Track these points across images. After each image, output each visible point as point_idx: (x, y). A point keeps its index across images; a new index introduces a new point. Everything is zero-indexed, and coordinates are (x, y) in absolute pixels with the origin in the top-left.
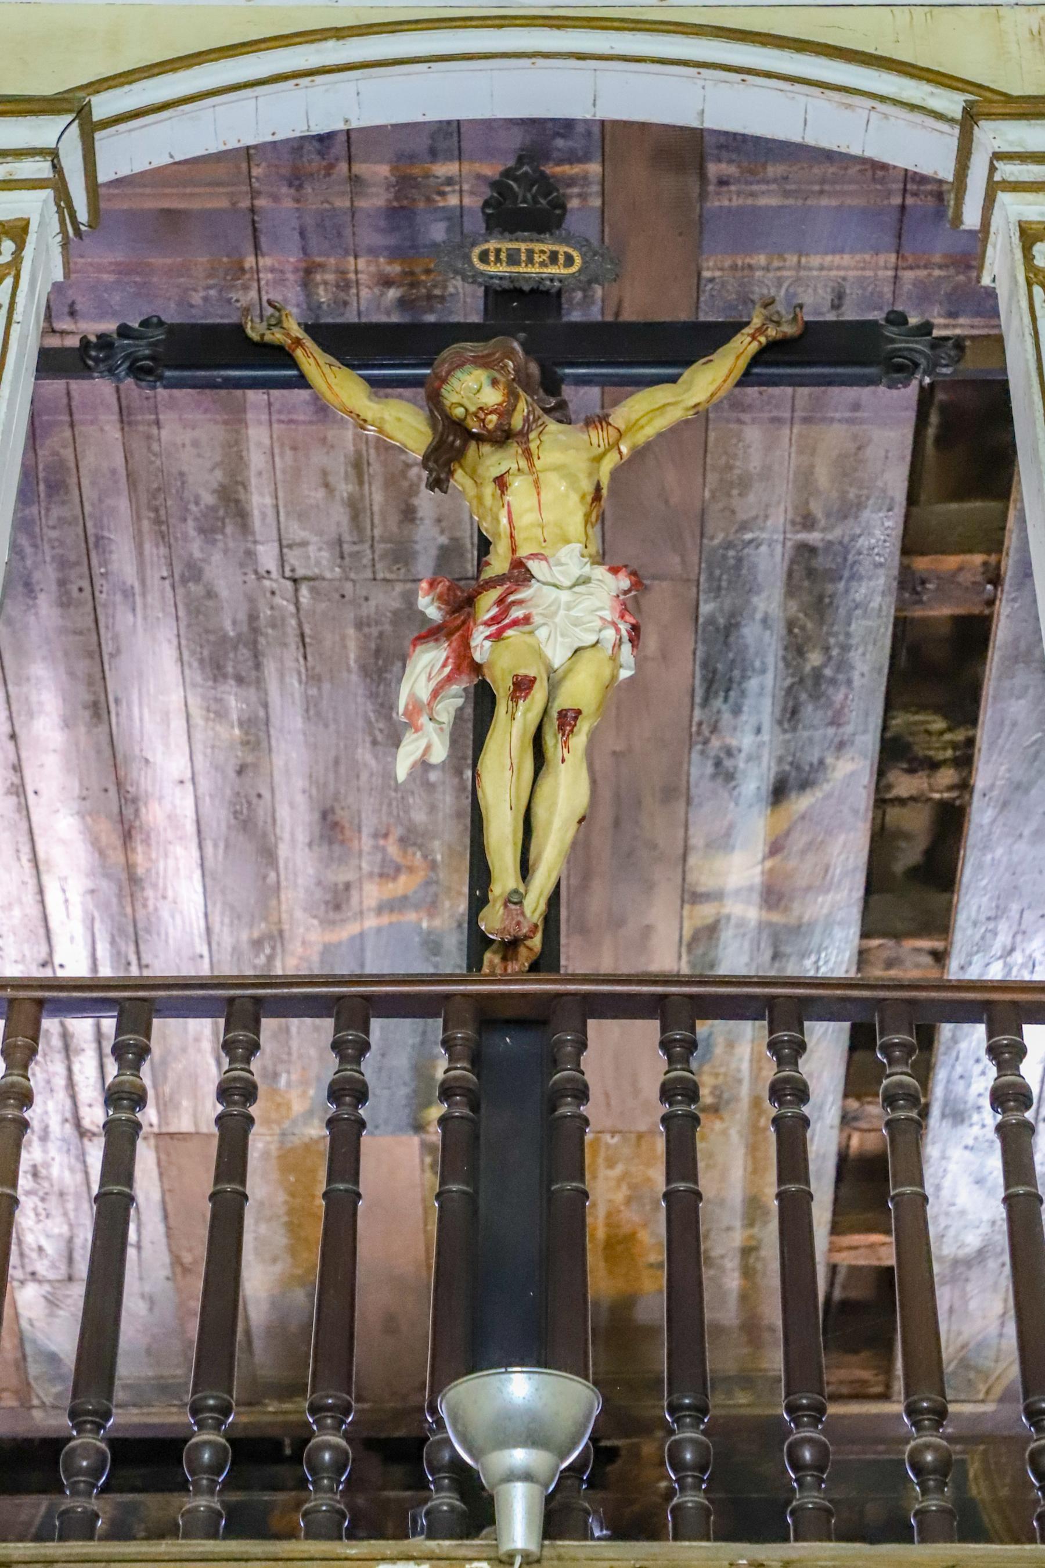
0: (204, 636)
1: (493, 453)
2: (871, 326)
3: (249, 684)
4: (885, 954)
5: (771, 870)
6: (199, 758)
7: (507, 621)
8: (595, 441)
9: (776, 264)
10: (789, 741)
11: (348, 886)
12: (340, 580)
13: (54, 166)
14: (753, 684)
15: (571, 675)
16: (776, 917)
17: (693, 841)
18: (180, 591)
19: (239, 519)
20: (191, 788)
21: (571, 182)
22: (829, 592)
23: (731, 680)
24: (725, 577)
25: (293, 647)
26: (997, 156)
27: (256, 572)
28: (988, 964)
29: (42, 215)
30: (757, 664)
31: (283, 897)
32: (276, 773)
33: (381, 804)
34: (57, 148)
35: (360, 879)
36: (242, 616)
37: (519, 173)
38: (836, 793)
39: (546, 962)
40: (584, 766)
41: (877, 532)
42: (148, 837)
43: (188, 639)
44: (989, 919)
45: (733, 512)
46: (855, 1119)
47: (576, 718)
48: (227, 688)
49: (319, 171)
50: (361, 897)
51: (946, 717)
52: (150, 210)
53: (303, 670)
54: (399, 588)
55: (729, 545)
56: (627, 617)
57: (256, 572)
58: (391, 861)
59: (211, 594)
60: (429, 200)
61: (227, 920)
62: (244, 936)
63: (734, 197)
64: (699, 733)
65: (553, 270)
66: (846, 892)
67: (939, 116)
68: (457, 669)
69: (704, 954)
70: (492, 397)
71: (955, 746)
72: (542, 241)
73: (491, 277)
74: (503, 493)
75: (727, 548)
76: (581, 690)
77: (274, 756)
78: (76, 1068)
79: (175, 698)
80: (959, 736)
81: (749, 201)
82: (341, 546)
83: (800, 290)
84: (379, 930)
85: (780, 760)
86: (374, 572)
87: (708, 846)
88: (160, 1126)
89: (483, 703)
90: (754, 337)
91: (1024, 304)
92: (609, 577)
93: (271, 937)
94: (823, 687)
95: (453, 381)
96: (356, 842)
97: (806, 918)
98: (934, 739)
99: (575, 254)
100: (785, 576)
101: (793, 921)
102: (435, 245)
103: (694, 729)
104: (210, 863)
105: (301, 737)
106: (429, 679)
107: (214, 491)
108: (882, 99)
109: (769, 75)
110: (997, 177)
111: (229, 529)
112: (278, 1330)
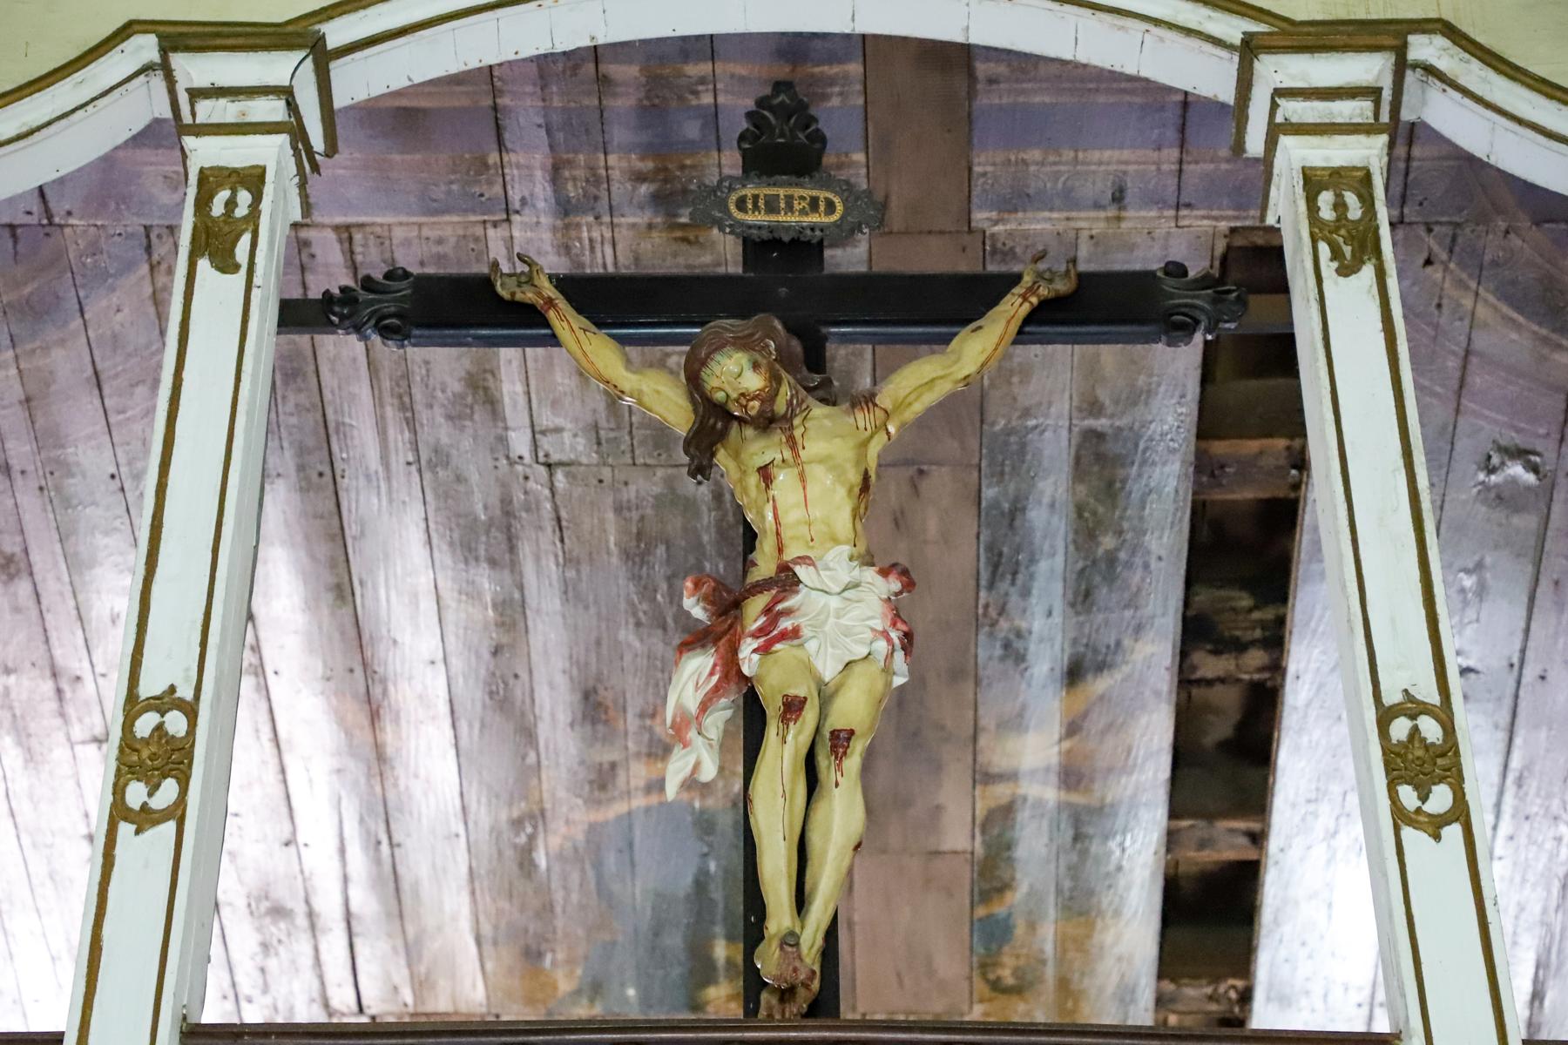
4: (1198, 833)
5: (1069, 752)
6: (451, 639)
8: (861, 424)
9: (1051, 158)
11: (613, 766)
13: (288, 104)
14: (1043, 566)
16: (1077, 798)
17: (983, 722)
18: (427, 476)
21: (832, 81)
25: (549, 530)
26: (1279, 93)
27: (508, 457)
28: (1309, 848)
29: (279, 163)
30: (1046, 547)
31: (544, 777)
32: (533, 655)
34: (291, 87)
35: (627, 759)
36: (494, 501)
37: (776, 101)
38: (1136, 675)
39: (824, 1005)
40: (859, 790)
41: (1170, 419)
44: (1309, 801)
45: (1015, 399)
46: (1173, 1000)
47: (849, 739)
48: (481, 570)
51: (1253, 594)
55: (1008, 432)
56: (900, 625)
57: (508, 457)
58: (660, 741)
59: (459, 479)
60: (681, 98)
61: (484, 800)
62: (504, 816)
64: (985, 614)
65: (814, 218)
67: (1217, 42)
68: (725, 677)
69: (1000, 835)
70: (754, 382)
71: (1263, 625)
72: (801, 186)
73: (750, 227)
74: (767, 487)
75: (1009, 435)
78: (323, 947)
79: (424, 580)
80: (1268, 614)
81: (1021, 99)
84: (648, 810)
85: (1075, 641)
86: (633, 458)
87: (998, 726)
88: (415, 1005)
89: (753, 721)
90: (1025, 299)
91: (1309, 264)
92: (879, 579)
93: (532, 817)
95: (712, 364)
97: (1109, 800)
98: (1241, 617)
99: (837, 200)
100: (1072, 462)
103: (981, 611)
104: (464, 742)
105: (559, 619)
106: (697, 688)
110: (1279, 119)
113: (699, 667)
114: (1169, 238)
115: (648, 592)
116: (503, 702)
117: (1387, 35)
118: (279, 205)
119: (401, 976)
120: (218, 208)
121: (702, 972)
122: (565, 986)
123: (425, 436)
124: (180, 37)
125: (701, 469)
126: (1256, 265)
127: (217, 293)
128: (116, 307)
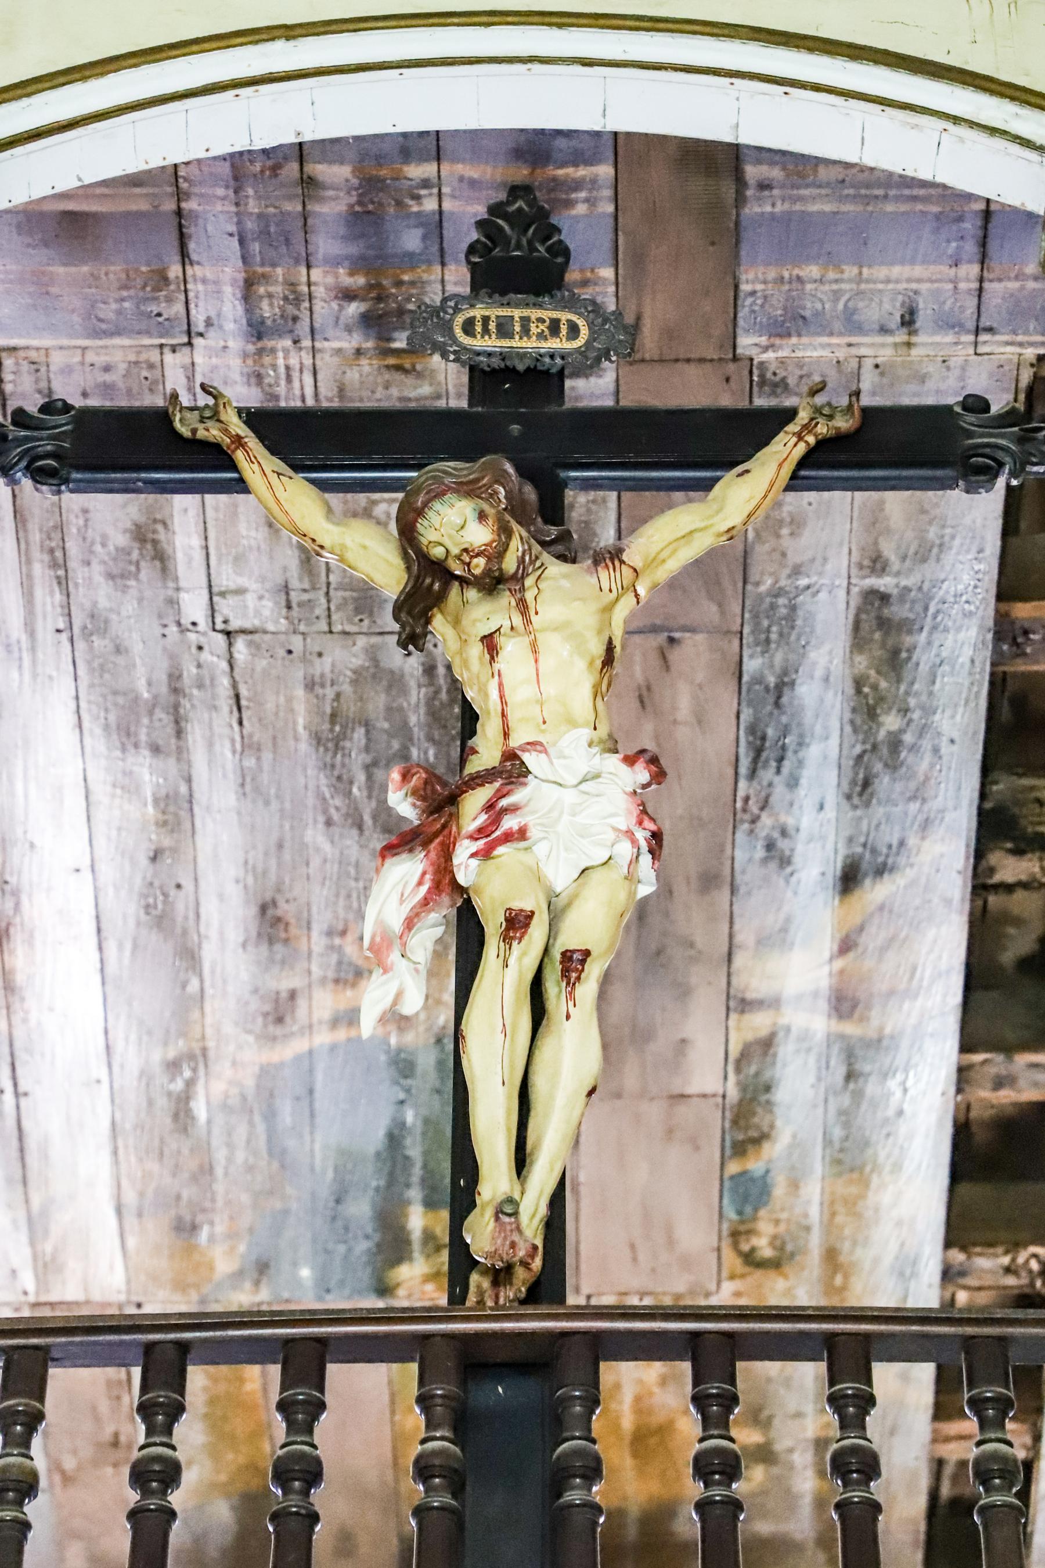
0: (110, 697)
1: (480, 600)
2: (942, 412)
3: (168, 755)
4: (993, 1070)
5: (842, 972)
6: (100, 842)
7: (498, 833)
8: (605, 586)
9: (831, 275)
10: (860, 818)
11: (293, 995)
12: (286, 633)
15: (576, 903)
16: (850, 1029)
17: (739, 938)
18: (80, 645)
19: (157, 563)
20: (90, 876)
21: (577, 185)
22: (907, 645)
23: (784, 748)
24: (774, 629)
25: (226, 709)
27: (179, 624)
31: (208, 1008)
33: (337, 895)
35: (310, 986)
39: (547, 1287)
41: (966, 577)
42: (31, 936)
43: (89, 702)
46: (962, 1274)
47: (583, 962)
49: (262, 172)
50: (310, 1007)
52: (52, 212)
53: (238, 738)
54: (362, 641)
55: (778, 593)
57: (179, 624)
58: (350, 964)
60: (399, 203)
61: (133, 1037)
62: (157, 1056)
63: (779, 203)
66: (939, 998)
68: (437, 887)
69: (757, 1074)
70: (480, 535)
73: (478, 354)
74: (492, 658)
75: (776, 596)
77: (199, 838)
81: (798, 207)
82: (287, 594)
83: (861, 305)
84: (333, 1048)
85: (850, 840)
87: (760, 942)
88: (37, 1293)
90: (800, 438)
93: (191, 1057)
94: (903, 755)
96: (304, 940)
97: (888, 1030)
99: (581, 323)
100: (850, 626)
101: (871, 1033)
102: (411, 255)
104: (111, 968)
106: (402, 901)
107: (125, 531)
108: (956, 120)
109: (817, 88)
111: (143, 575)
113: (409, 871)
115: (342, 783)
116: (165, 919)
121: (393, 1246)
122: (224, 1265)
123: (81, 597)
125: (413, 639)
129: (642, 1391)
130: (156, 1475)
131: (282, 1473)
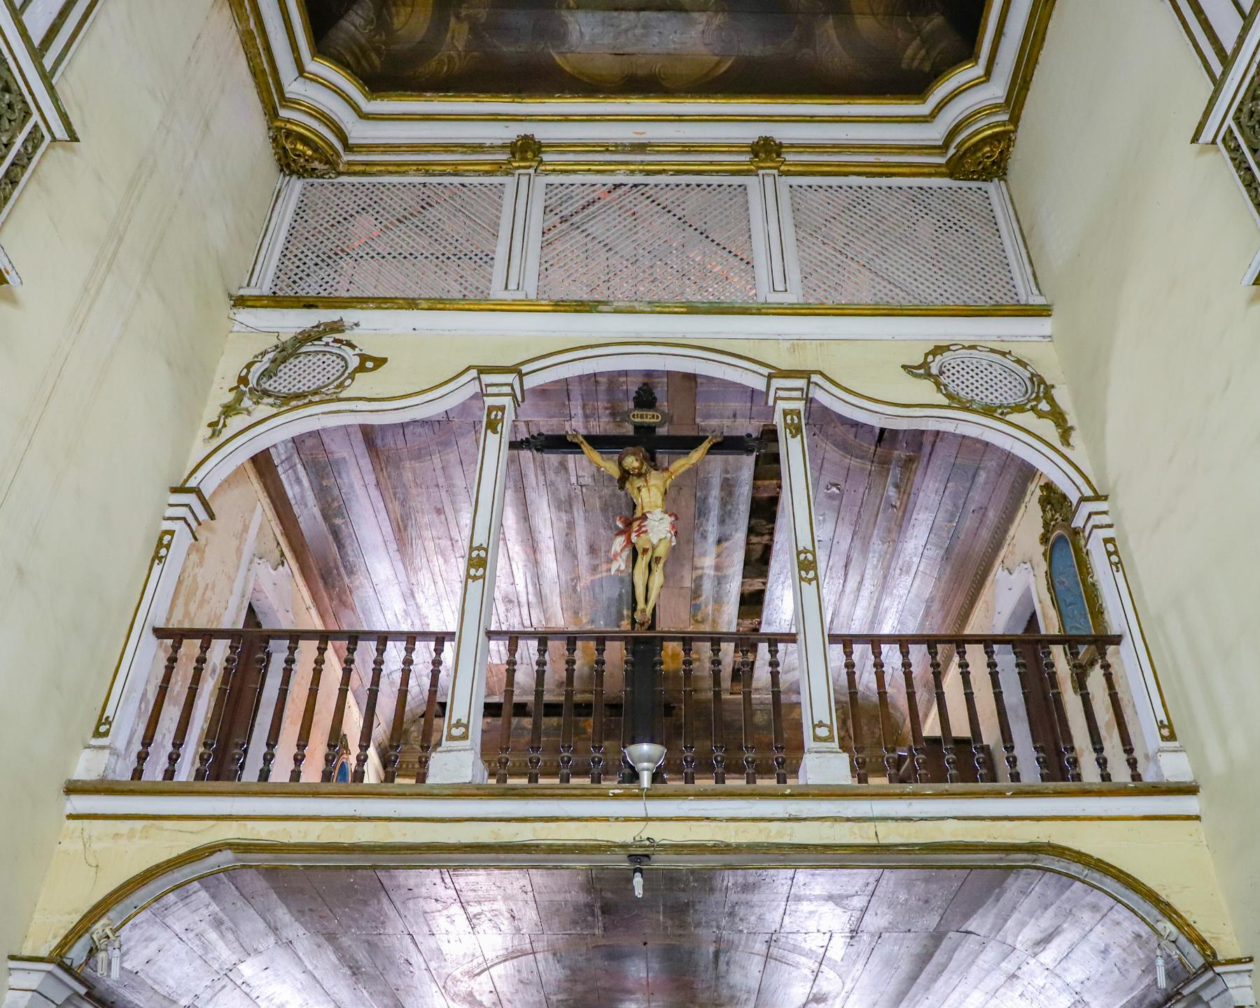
2: (742, 437)
39: (652, 627)
70: (636, 464)
76: (661, 551)
112: (581, 678)
113: (620, 540)
114: (748, 427)
115: (607, 519)
116: (568, 548)
117: (805, 374)
118: (509, 416)
119: (542, 618)
120: (493, 417)
121: (620, 617)
122: (585, 621)
123: (548, 478)
124: (482, 370)
125: (622, 488)
126: (770, 435)
127: (493, 439)
128: (466, 442)
129: (672, 647)
130: (570, 662)
131: (597, 663)
